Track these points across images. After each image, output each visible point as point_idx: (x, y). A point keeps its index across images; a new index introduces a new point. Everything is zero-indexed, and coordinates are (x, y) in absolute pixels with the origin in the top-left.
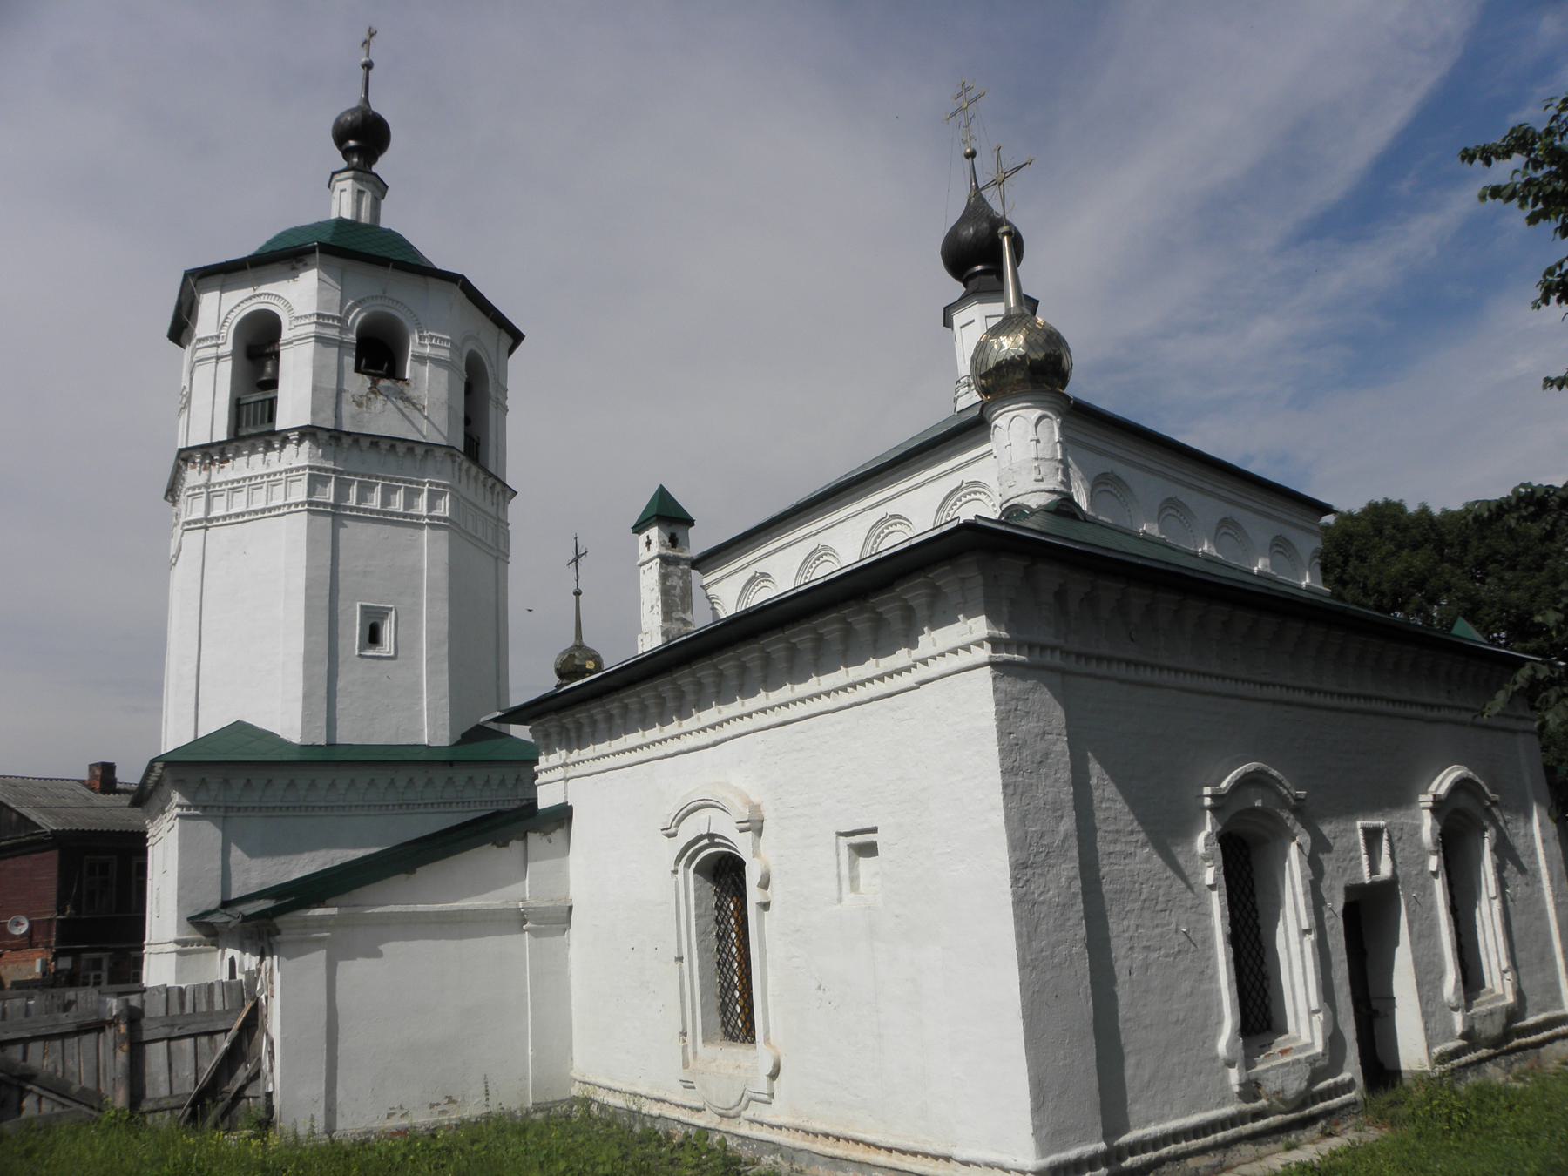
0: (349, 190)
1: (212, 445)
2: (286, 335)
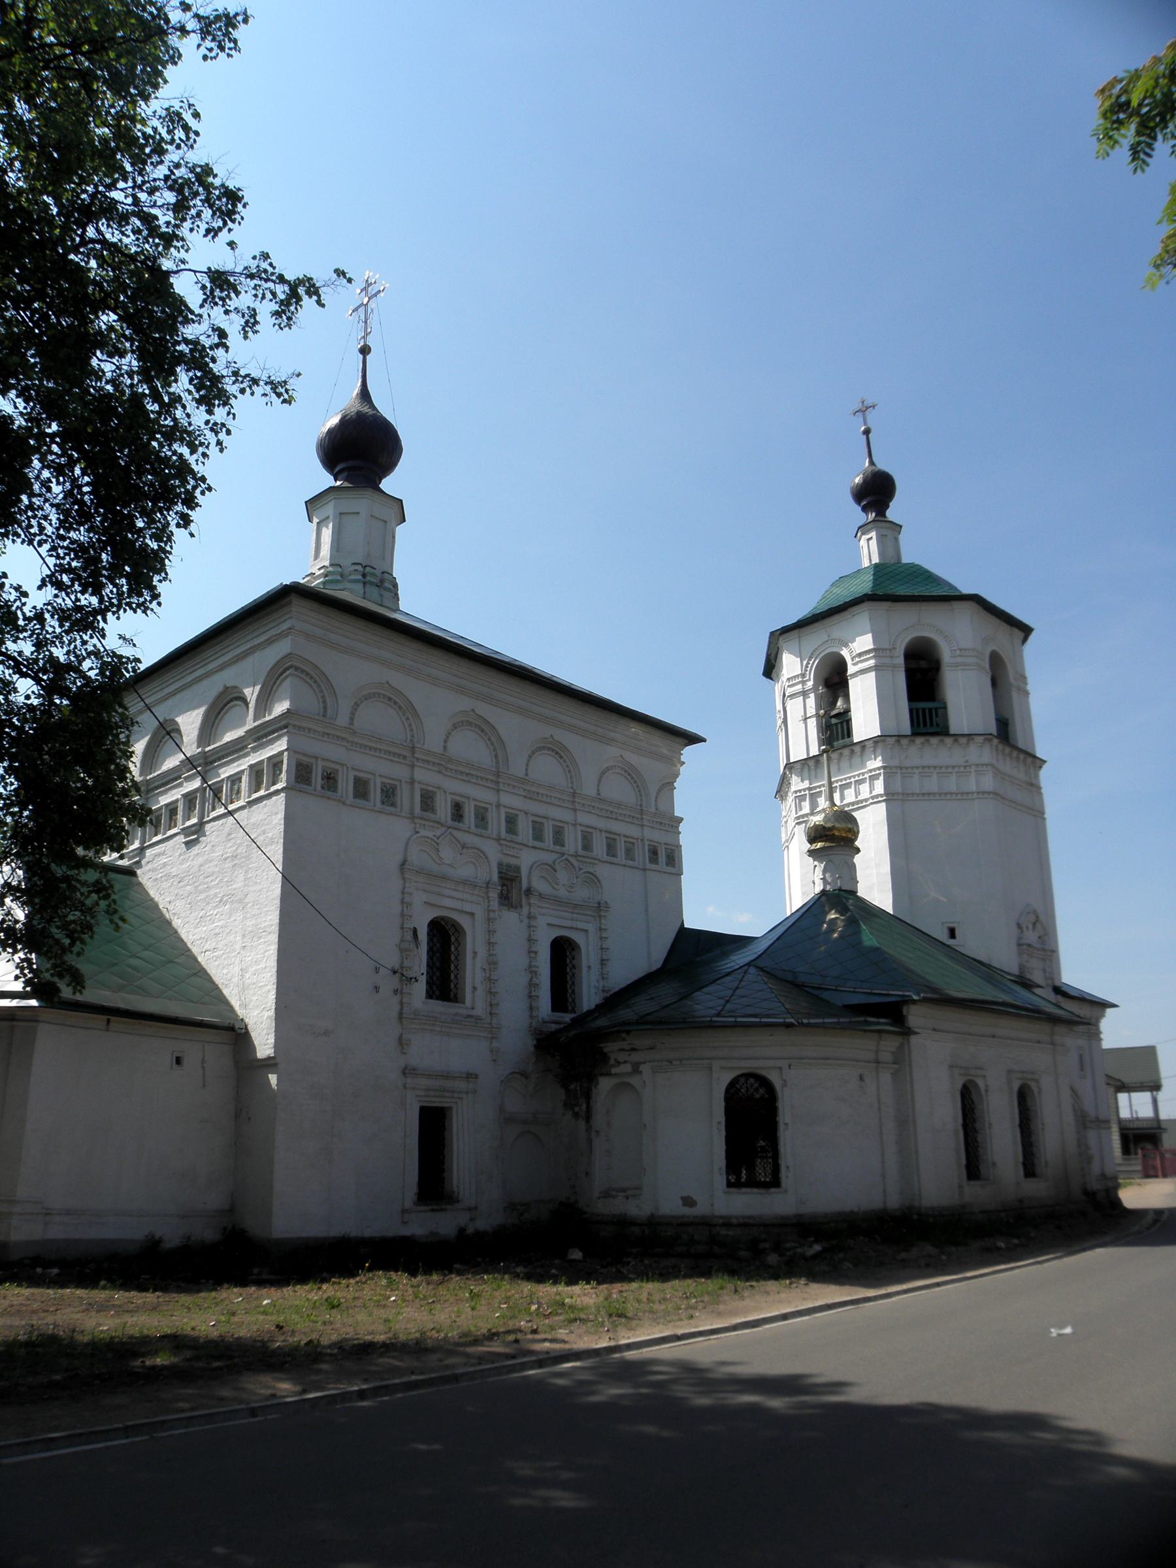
0: (874, 538)
1: (809, 758)
2: (851, 669)
